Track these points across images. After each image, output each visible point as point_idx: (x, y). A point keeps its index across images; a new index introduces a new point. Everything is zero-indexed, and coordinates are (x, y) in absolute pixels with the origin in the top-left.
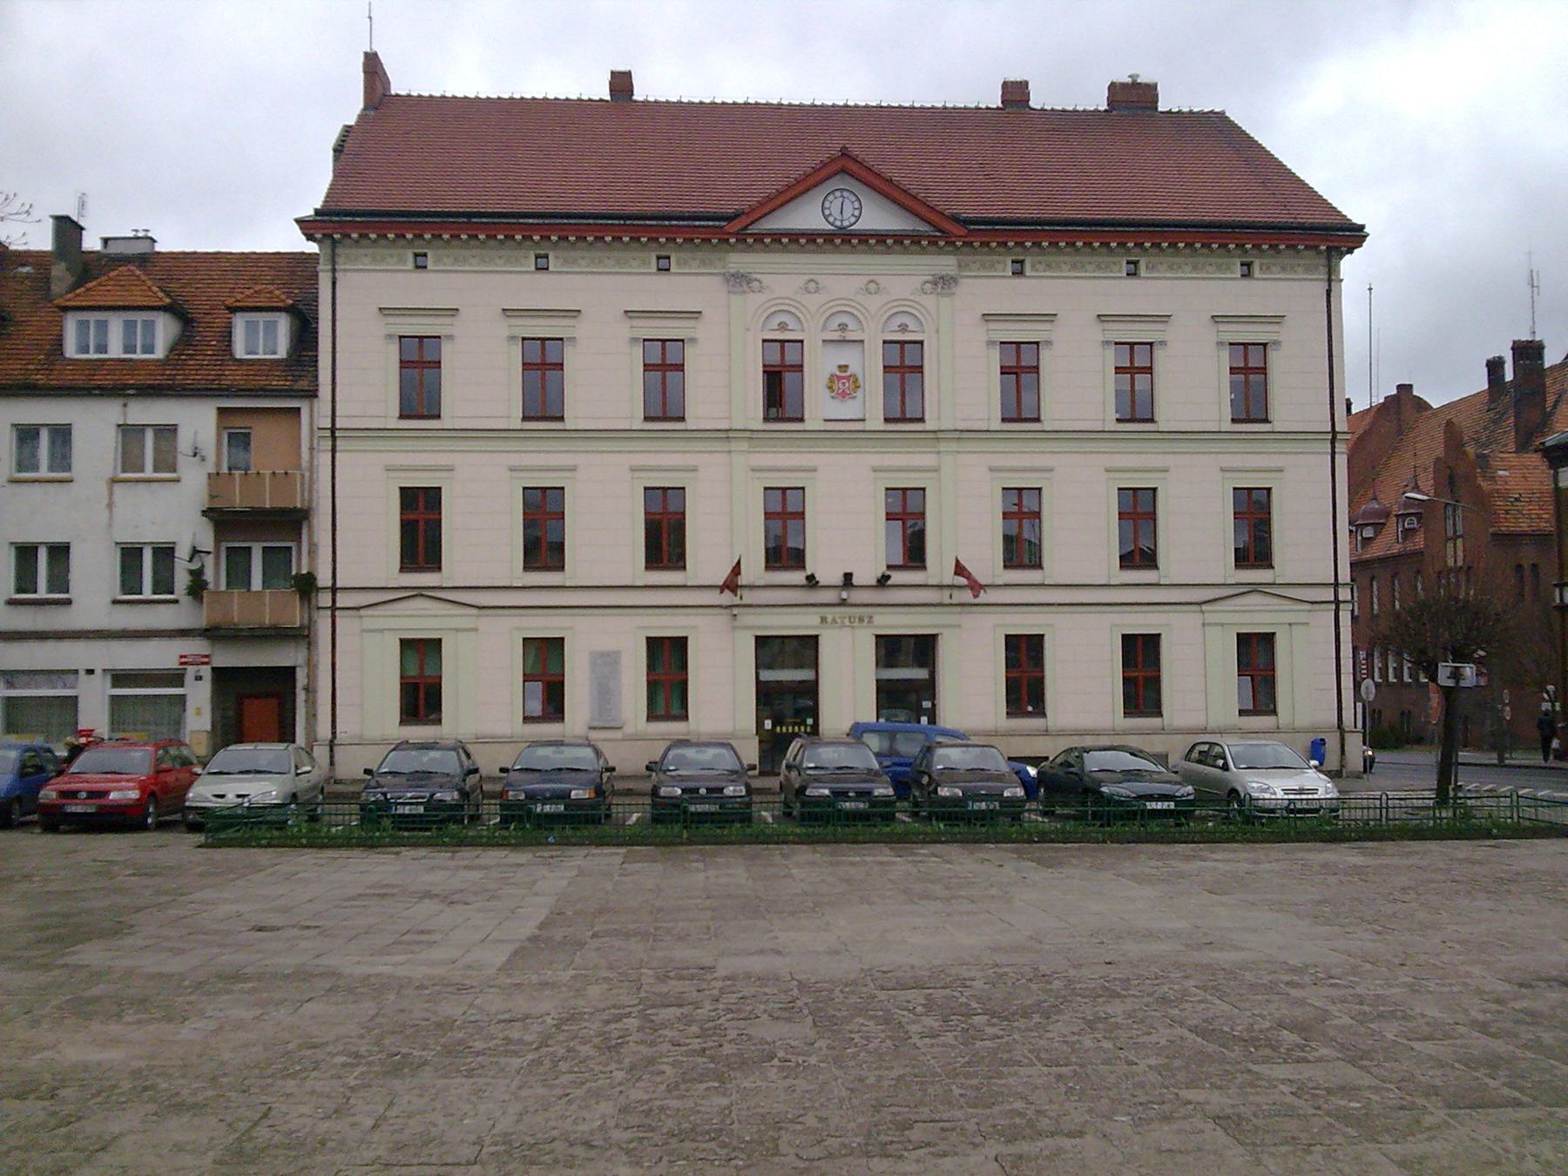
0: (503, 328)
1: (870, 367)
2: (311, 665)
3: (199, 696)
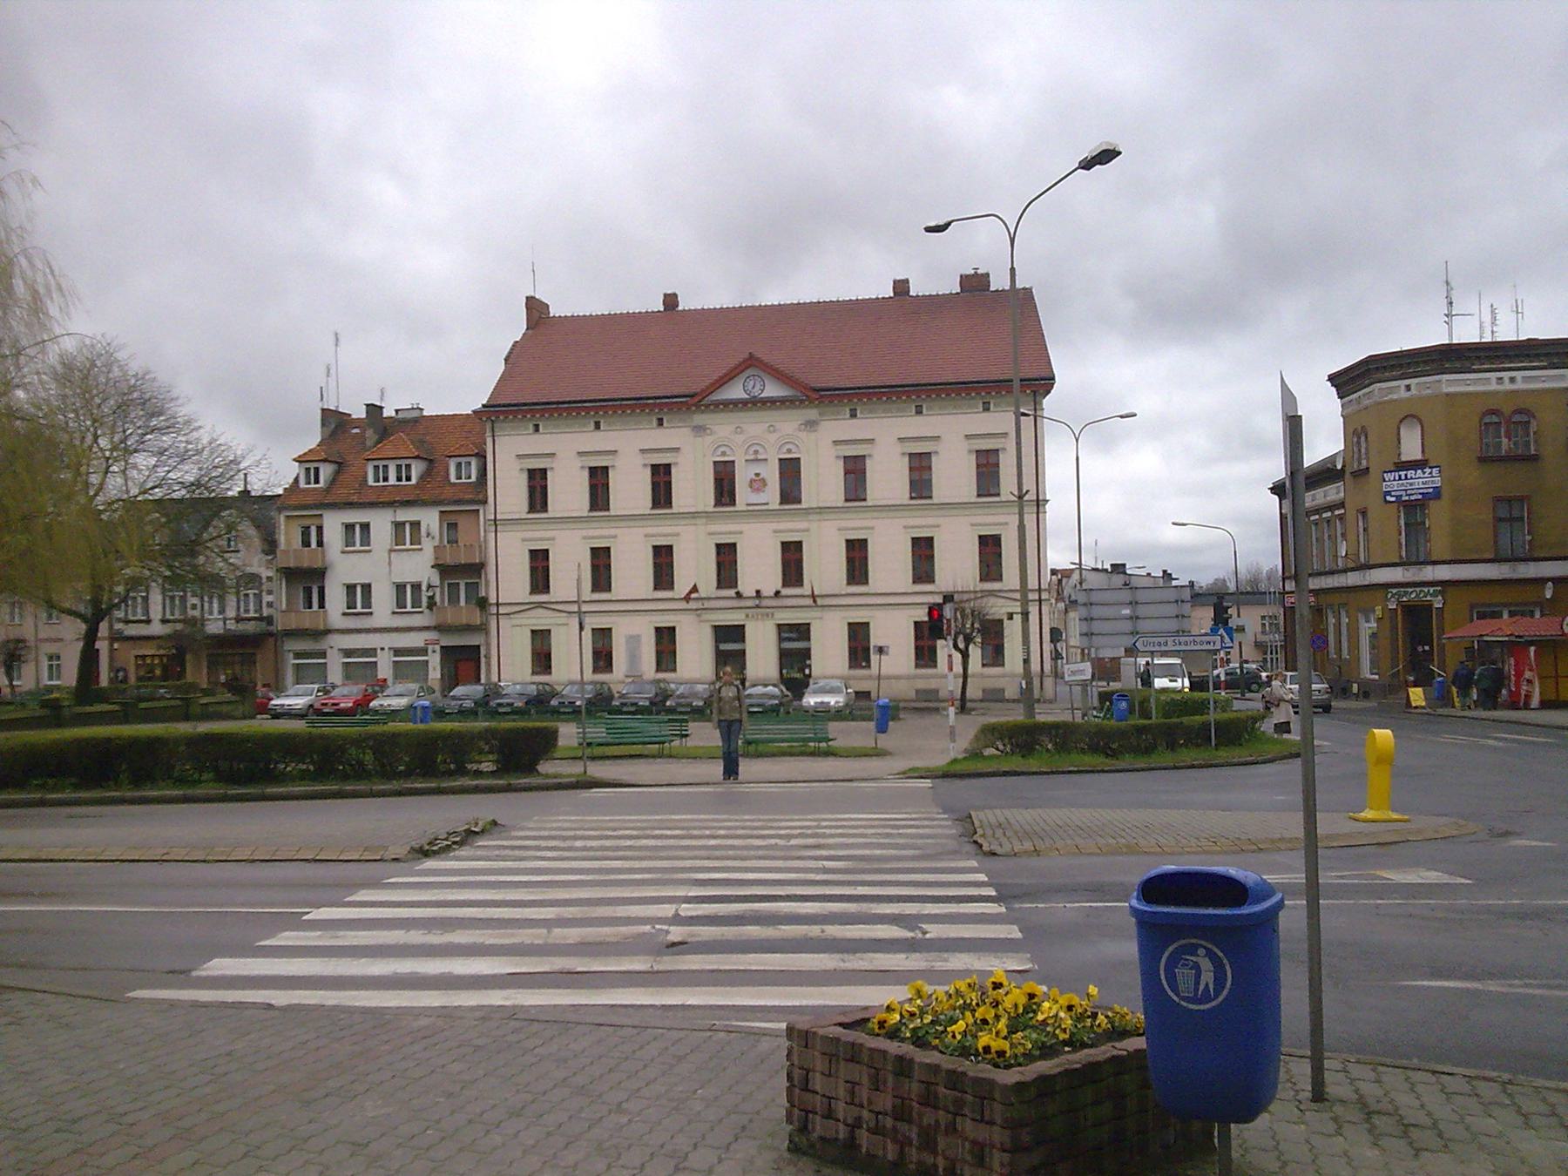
0: (578, 462)
1: (772, 474)
2: (488, 645)
3: (434, 660)
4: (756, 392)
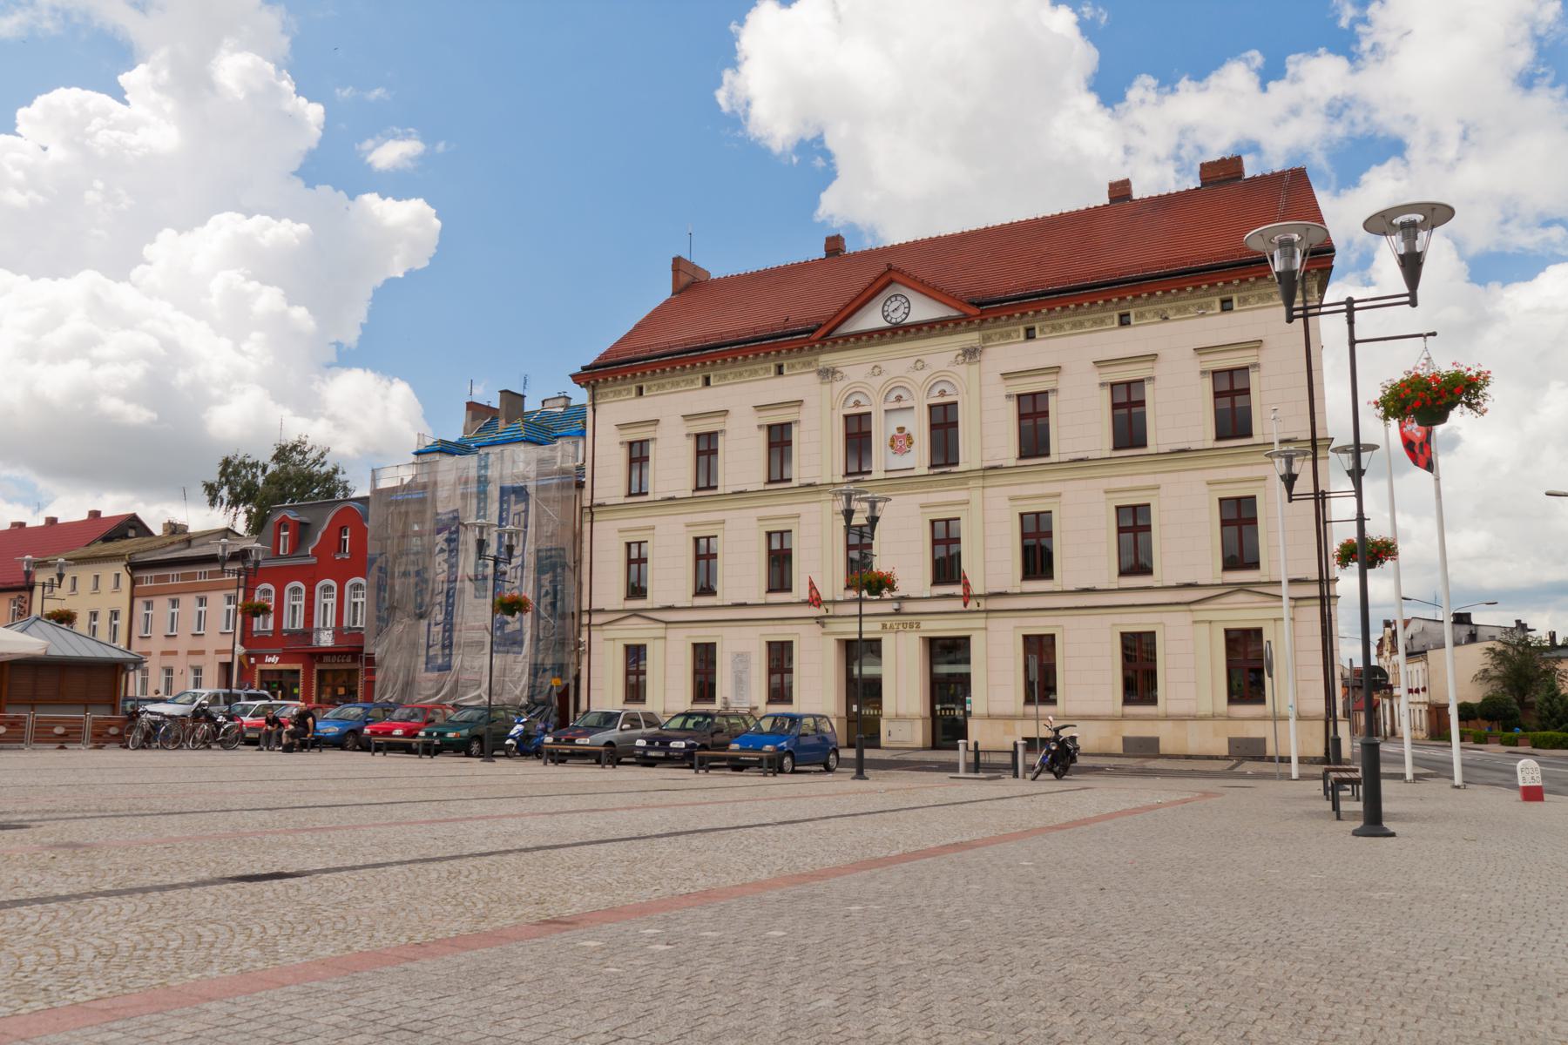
4: (897, 317)
